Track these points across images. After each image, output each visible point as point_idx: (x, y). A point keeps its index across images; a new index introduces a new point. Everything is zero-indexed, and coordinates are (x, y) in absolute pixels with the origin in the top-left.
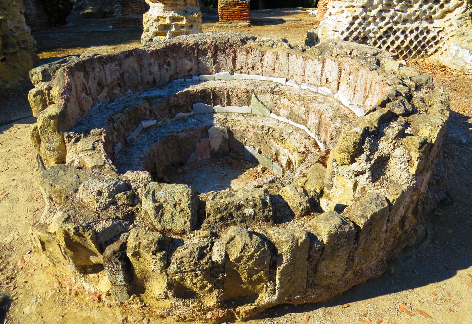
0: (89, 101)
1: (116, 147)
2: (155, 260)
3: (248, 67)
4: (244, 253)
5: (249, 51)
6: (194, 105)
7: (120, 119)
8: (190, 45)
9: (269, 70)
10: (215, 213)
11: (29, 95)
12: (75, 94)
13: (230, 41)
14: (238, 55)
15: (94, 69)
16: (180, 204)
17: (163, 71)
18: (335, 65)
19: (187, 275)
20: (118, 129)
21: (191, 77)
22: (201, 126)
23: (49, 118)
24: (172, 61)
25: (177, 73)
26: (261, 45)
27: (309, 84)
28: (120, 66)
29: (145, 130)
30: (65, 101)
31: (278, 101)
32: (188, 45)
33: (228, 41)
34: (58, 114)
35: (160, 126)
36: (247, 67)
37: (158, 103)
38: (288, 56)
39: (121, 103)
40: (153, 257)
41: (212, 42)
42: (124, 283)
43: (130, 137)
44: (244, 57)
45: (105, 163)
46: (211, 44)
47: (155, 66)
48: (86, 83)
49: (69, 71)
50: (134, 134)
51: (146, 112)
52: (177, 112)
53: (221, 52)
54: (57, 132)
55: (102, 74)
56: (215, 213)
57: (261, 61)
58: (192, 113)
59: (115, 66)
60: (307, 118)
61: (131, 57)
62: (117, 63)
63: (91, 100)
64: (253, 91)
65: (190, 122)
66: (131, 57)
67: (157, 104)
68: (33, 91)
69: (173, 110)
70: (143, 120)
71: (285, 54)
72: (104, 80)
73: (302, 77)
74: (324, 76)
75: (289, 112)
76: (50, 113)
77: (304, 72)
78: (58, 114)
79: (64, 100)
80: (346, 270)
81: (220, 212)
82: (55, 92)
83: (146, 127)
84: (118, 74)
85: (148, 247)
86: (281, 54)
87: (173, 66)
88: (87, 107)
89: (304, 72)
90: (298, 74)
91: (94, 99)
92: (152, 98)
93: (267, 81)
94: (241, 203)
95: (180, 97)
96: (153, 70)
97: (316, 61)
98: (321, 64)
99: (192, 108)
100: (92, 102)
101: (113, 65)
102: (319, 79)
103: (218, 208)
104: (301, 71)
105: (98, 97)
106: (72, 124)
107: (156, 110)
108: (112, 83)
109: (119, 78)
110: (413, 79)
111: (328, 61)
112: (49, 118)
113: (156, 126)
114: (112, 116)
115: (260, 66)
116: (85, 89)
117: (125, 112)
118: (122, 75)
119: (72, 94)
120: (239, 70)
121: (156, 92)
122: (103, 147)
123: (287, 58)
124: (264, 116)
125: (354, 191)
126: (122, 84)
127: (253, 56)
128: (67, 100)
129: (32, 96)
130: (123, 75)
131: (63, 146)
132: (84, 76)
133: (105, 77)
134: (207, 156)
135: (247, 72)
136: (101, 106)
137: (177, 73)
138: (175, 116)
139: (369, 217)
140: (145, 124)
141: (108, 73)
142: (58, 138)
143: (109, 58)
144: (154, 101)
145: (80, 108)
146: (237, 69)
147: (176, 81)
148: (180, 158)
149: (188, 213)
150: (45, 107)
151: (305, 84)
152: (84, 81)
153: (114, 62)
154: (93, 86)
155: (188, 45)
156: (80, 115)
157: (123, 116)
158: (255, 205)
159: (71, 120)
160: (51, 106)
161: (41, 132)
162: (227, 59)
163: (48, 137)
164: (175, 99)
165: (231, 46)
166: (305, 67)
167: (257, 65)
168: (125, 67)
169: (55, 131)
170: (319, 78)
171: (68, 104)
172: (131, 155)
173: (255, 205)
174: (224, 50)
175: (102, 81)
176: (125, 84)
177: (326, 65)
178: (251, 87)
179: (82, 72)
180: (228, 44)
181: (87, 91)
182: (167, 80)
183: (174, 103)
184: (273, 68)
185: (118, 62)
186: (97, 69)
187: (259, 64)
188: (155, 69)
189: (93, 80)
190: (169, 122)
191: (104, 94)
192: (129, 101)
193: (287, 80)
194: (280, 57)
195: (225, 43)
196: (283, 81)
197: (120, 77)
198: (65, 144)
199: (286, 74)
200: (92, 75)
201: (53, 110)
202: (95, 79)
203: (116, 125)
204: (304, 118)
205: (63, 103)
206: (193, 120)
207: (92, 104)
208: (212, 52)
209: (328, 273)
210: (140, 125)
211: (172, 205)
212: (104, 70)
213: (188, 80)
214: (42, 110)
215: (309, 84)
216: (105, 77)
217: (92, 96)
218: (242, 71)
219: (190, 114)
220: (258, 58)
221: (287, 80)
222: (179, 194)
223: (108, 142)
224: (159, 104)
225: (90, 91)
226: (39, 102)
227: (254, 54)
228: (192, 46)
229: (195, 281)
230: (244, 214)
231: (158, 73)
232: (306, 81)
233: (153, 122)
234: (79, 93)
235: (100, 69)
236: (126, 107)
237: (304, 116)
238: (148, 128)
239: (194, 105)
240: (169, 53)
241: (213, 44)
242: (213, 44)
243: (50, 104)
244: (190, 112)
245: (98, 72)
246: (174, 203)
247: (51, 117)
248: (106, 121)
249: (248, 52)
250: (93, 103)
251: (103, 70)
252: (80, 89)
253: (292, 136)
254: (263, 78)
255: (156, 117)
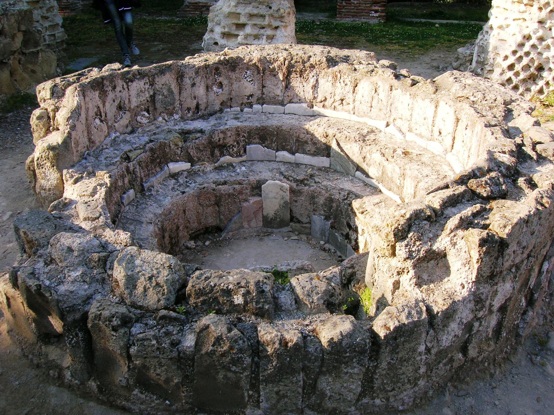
0: (102, 130)
1: (125, 196)
2: (114, 338)
3: (334, 100)
4: (217, 348)
5: (336, 76)
6: (248, 147)
7: (138, 158)
8: (254, 62)
9: (364, 108)
10: (197, 294)
11: (32, 115)
12: (85, 119)
13: (311, 59)
14: (321, 81)
15: (114, 88)
16: (158, 277)
17: (212, 96)
18: (452, 111)
19: (150, 362)
20: (134, 171)
21: (250, 105)
22: (252, 178)
23: (48, 149)
24: (225, 82)
25: (231, 99)
26: (355, 70)
27: (416, 134)
28: (152, 85)
29: (174, 176)
30: (70, 128)
31: (368, 156)
32: (250, 61)
33: (309, 60)
34: (60, 143)
35: (195, 173)
36: (332, 100)
37: (196, 139)
38: (391, 90)
39: (145, 135)
40: (113, 333)
41: (285, 60)
42: (84, 360)
43: (148, 184)
44: (330, 84)
45: (100, 215)
46: (283, 62)
47: (201, 87)
48: (101, 106)
49: (81, 90)
50: (155, 181)
51: (177, 150)
52: (222, 155)
53: (296, 74)
54: (55, 167)
55: (125, 94)
56: (197, 294)
57: (354, 92)
58: (244, 158)
59: (144, 84)
60: (403, 185)
61: (168, 73)
62: (148, 81)
63: (105, 128)
64: (334, 136)
65: (238, 171)
66: (168, 73)
67: (194, 141)
68: (37, 112)
69: (217, 152)
70: (172, 161)
71: (387, 87)
72: (127, 102)
73: (408, 123)
74: (436, 125)
75: (380, 173)
76: (51, 143)
77: (411, 115)
78: (60, 143)
79: (68, 126)
80: (360, 395)
81: (202, 295)
82: (61, 116)
83: (174, 172)
84: (148, 95)
85: (109, 321)
86: (381, 86)
87: (226, 89)
88: (98, 137)
89: (411, 115)
90: (404, 118)
91: (109, 128)
92: (189, 132)
93: (358, 122)
94: (230, 287)
95: (229, 134)
96: (197, 92)
97: (427, 101)
98: (433, 107)
99: (245, 151)
100: (107, 132)
101: (142, 83)
102: (430, 129)
103: (200, 289)
104: (407, 114)
105: (116, 125)
106: (75, 158)
107: (192, 149)
108: (137, 107)
109: (148, 101)
110: (538, 147)
111: (442, 104)
112: (48, 149)
113: (188, 172)
114: (128, 153)
115: (352, 100)
116: (98, 114)
117: (147, 148)
118: (153, 97)
119: (80, 120)
120: (321, 102)
121: (198, 124)
122: (104, 193)
123: (390, 92)
124: (348, 174)
125: (392, 295)
126: (151, 109)
127: (343, 84)
128: (73, 128)
129: (35, 118)
130: (155, 98)
131: (61, 186)
132: (100, 98)
133: (129, 99)
134: (257, 223)
135: (333, 106)
136: (117, 137)
137: (231, 99)
138: (219, 160)
139: (392, 329)
140: (174, 167)
141: (133, 92)
142: (56, 175)
143: (137, 73)
144: (191, 136)
145: (90, 139)
146: (319, 100)
147: (229, 110)
148: (218, 221)
149: (164, 290)
150: (48, 131)
151: (411, 134)
152: (99, 103)
153: (143, 79)
154: (110, 108)
155: (251, 61)
156: (87, 147)
157: (142, 155)
158: (248, 292)
159: (75, 154)
160: (54, 133)
161: (38, 164)
162: (305, 84)
163: (44, 173)
164: (221, 136)
165: (312, 67)
166: (412, 109)
167: (347, 98)
168: (158, 86)
169: (53, 166)
170: (430, 127)
171: (73, 133)
172: (145, 208)
173: (248, 292)
174: (301, 71)
175: (124, 104)
176: (155, 109)
177: (439, 109)
178: (333, 129)
179: (98, 92)
180: (307, 65)
181: (101, 116)
182: (217, 107)
183: (219, 141)
184: (370, 105)
185: (149, 79)
186: (118, 89)
187: (349, 97)
188: (201, 91)
189: (112, 102)
190: (209, 167)
191: (125, 119)
192: (158, 134)
193: (388, 125)
194: (380, 91)
195: (304, 62)
196: (380, 125)
197: (149, 100)
198: (64, 183)
199: (387, 116)
200: (111, 95)
201: (56, 138)
202: (114, 101)
203: (131, 165)
204: (399, 184)
205: (66, 131)
206: (244, 168)
207: (106, 133)
208: (284, 74)
209: (332, 394)
210: (166, 168)
211: (147, 277)
212: (128, 89)
213: (246, 110)
214: (44, 136)
215: (416, 134)
216: (129, 99)
217: (107, 123)
218: (326, 103)
219: (241, 159)
220: (350, 88)
221: (388, 125)
222: (160, 265)
223: (116, 188)
224: (197, 141)
225: (106, 116)
226: (42, 127)
227: (344, 81)
228: (256, 63)
229: (158, 371)
230: (232, 301)
231: (204, 97)
232: (414, 129)
233: (186, 166)
234: (90, 118)
235: (123, 88)
236: (151, 141)
237: (398, 181)
238: (178, 173)
239: (248, 147)
240: (223, 70)
241: (287, 62)
242: (287, 62)
243: (54, 129)
244: (241, 156)
245: (120, 91)
246: (150, 275)
247: (51, 148)
248: (118, 159)
249: (335, 77)
250: (108, 132)
251: (127, 89)
252: (92, 113)
253: (377, 210)
254: (354, 118)
255: (190, 160)
